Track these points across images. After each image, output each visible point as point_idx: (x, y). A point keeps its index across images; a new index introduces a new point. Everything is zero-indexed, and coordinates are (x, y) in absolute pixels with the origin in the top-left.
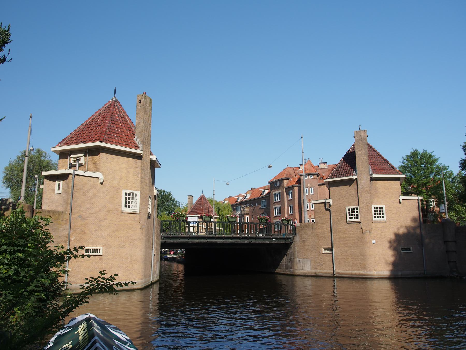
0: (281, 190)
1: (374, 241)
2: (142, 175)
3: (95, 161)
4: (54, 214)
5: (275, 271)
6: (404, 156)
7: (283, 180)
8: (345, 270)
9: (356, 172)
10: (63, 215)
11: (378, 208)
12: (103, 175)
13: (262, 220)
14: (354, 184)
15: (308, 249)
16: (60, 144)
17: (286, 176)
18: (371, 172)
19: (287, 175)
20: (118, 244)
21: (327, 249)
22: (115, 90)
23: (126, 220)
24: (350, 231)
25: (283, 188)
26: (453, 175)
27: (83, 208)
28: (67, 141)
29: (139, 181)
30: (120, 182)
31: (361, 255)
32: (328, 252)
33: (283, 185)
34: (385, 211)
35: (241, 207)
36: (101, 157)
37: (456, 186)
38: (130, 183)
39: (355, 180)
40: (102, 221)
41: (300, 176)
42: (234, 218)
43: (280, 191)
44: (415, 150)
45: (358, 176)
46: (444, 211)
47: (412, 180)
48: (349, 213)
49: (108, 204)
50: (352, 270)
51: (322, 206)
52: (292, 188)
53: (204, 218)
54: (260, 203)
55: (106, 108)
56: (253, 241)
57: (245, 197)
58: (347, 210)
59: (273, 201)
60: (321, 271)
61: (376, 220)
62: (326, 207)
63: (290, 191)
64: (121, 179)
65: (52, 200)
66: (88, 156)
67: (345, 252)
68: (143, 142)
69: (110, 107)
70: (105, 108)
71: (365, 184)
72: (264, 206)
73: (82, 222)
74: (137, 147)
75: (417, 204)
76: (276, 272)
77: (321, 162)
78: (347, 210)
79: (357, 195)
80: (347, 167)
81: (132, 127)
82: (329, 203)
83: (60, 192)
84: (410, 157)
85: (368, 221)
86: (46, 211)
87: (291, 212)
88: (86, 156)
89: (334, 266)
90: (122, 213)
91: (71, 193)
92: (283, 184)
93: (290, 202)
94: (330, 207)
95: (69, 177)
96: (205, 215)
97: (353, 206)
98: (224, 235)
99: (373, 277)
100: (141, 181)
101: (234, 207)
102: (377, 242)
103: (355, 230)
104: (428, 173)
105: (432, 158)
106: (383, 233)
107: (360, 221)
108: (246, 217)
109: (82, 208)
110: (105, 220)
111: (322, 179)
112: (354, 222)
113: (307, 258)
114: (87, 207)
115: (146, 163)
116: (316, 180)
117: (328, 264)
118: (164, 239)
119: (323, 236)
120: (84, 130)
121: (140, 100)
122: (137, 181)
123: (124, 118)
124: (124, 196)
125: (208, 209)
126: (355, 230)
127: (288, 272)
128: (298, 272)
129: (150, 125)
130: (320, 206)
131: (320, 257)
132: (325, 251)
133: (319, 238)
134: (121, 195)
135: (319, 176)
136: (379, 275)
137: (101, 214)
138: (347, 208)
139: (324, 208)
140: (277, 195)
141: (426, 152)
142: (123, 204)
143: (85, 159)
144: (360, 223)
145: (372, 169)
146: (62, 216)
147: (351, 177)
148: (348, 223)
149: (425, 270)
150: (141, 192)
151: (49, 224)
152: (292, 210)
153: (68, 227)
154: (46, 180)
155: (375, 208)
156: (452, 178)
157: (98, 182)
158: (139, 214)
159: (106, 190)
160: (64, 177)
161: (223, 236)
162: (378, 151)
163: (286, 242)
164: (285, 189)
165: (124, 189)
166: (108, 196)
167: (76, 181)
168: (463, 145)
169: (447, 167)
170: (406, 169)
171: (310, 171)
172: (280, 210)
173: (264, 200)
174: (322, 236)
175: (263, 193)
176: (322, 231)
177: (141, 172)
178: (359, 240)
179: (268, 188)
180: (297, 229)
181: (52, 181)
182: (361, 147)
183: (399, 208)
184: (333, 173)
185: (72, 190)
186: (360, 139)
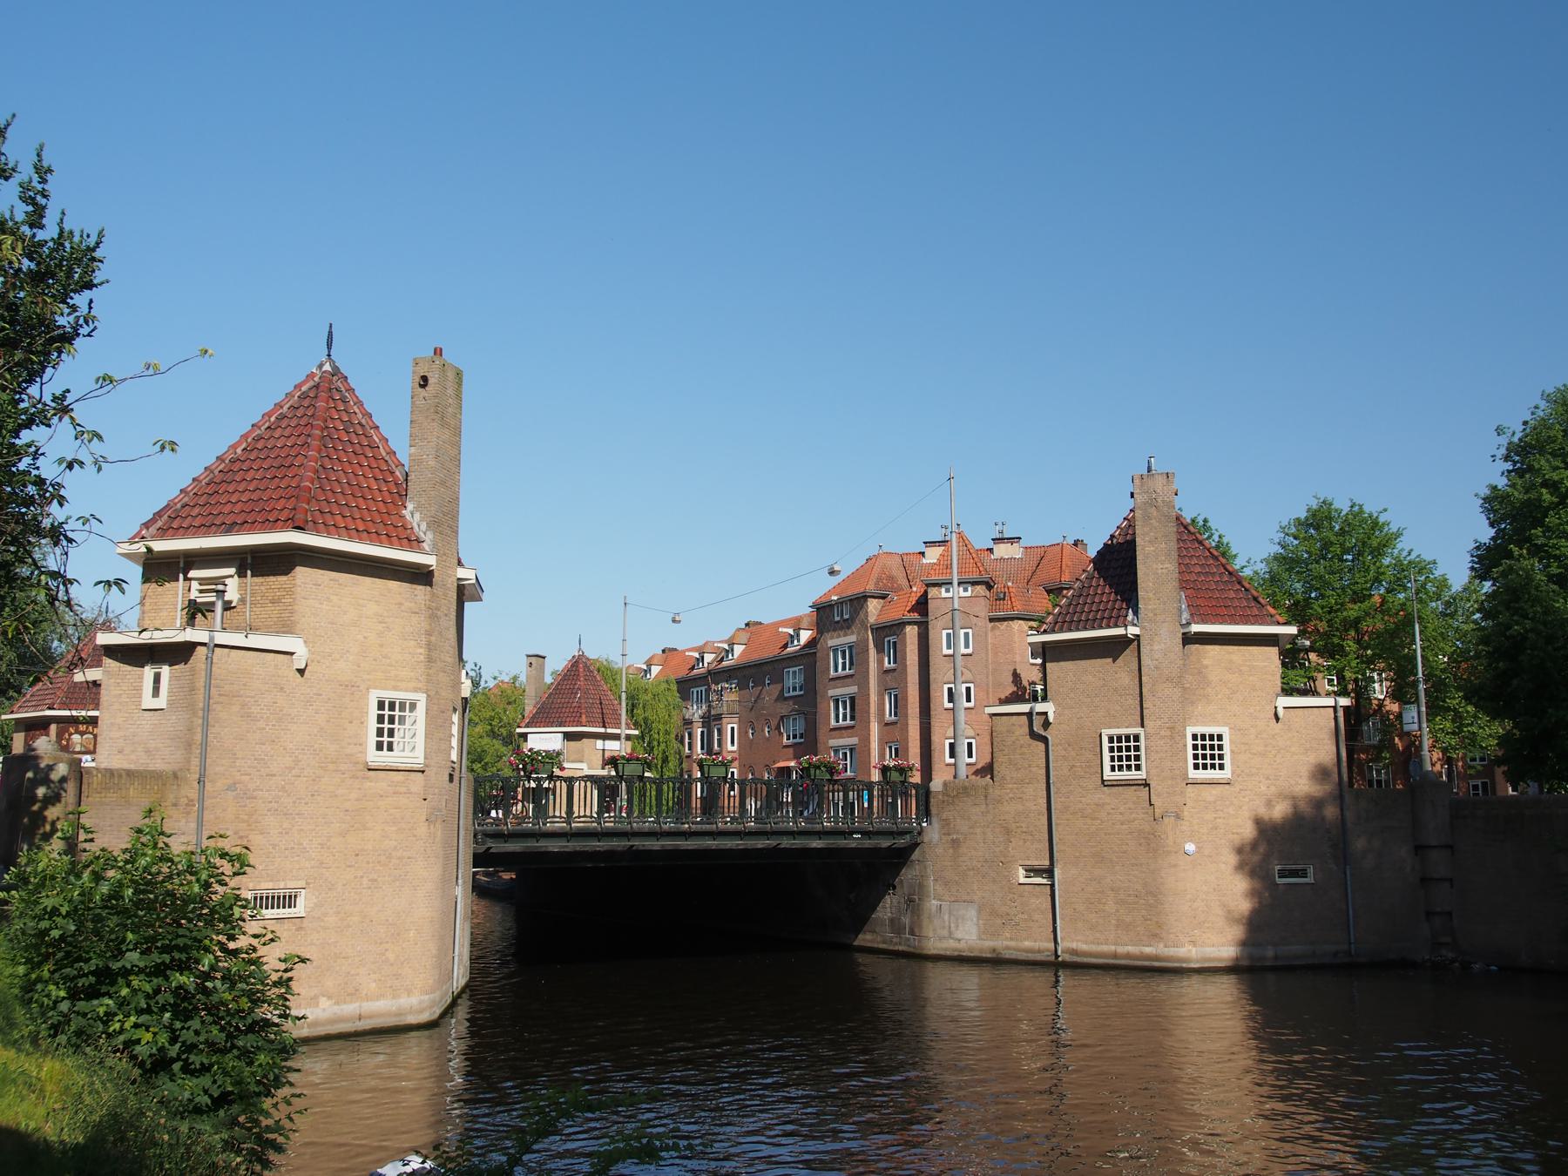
0: (859, 634)
1: (1190, 847)
2: (433, 639)
3: (278, 594)
4: (148, 782)
5: (854, 940)
9: (1136, 613)
10: (178, 785)
11: (1205, 735)
12: (305, 642)
13: (818, 771)
14: (1129, 654)
15: (969, 870)
16: (148, 528)
17: (877, 584)
18: (1186, 616)
19: (879, 579)
20: (356, 877)
21: (1032, 871)
22: (330, 333)
23: (381, 793)
24: (1112, 811)
25: (867, 626)
26: (1449, 588)
27: (243, 758)
28: (169, 517)
30: (362, 665)
33: (867, 619)
34: (1228, 738)
35: (708, 691)
36: (298, 582)
37: (1457, 630)
38: (392, 666)
40: (303, 801)
44: (1324, 502)
47: (1312, 609)
49: (324, 743)
51: (1021, 726)
52: (897, 627)
54: (778, 678)
55: (299, 397)
59: (829, 674)
60: (1012, 944)
61: (1197, 776)
62: (1035, 729)
64: (365, 652)
65: (131, 730)
66: (252, 576)
68: (435, 524)
69: (316, 397)
70: (296, 398)
72: (794, 689)
73: (240, 806)
74: (413, 543)
75: (1333, 724)
77: (1000, 536)
81: (394, 466)
82: (1046, 713)
83: (161, 702)
85: (1173, 778)
86: (124, 774)
88: (246, 576)
89: (1058, 928)
90: (369, 770)
91: (204, 710)
93: (889, 677)
94: (1045, 730)
95: (195, 653)
97: (1125, 730)
98: (688, 823)
99: (1184, 965)
100: (430, 660)
101: (686, 686)
103: (1130, 809)
107: (1145, 780)
108: (729, 726)
109: (238, 759)
110: (313, 795)
111: (1004, 599)
113: (968, 898)
114: (254, 755)
116: (983, 601)
117: (1037, 921)
119: (1022, 827)
120: (229, 477)
121: (425, 379)
122: (415, 659)
123: (366, 437)
124: (374, 712)
125: (601, 703)
126: (1130, 809)
127: (900, 944)
128: (934, 945)
129: (457, 461)
130: (1013, 725)
131: (1011, 896)
133: (1008, 832)
134: (365, 711)
135: (993, 587)
137: (300, 776)
138: (1106, 733)
139: (1027, 730)
140: (844, 652)
141: (1361, 511)
142: (373, 739)
143: (242, 588)
145: (1189, 606)
146: (175, 787)
147: (1119, 631)
148: (1105, 786)
150: (428, 696)
151: (244, 873)
152: (896, 707)
153: (193, 825)
154: (111, 661)
155: (1197, 735)
156: (1447, 598)
157: (287, 669)
158: (423, 772)
159: (314, 694)
160: (178, 653)
161: (687, 826)
163: (895, 843)
164: (872, 629)
165: (375, 688)
166: (323, 713)
167: (219, 668)
168: (1483, 496)
169: (1429, 563)
170: (1293, 569)
171: (964, 570)
173: (796, 669)
174: (1018, 825)
175: (792, 642)
176: (1020, 807)
177: (428, 627)
178: (1142, 841)
180: (932, 800)
181: (130, 665)
185: (205, 698)
186: (1152, 503)
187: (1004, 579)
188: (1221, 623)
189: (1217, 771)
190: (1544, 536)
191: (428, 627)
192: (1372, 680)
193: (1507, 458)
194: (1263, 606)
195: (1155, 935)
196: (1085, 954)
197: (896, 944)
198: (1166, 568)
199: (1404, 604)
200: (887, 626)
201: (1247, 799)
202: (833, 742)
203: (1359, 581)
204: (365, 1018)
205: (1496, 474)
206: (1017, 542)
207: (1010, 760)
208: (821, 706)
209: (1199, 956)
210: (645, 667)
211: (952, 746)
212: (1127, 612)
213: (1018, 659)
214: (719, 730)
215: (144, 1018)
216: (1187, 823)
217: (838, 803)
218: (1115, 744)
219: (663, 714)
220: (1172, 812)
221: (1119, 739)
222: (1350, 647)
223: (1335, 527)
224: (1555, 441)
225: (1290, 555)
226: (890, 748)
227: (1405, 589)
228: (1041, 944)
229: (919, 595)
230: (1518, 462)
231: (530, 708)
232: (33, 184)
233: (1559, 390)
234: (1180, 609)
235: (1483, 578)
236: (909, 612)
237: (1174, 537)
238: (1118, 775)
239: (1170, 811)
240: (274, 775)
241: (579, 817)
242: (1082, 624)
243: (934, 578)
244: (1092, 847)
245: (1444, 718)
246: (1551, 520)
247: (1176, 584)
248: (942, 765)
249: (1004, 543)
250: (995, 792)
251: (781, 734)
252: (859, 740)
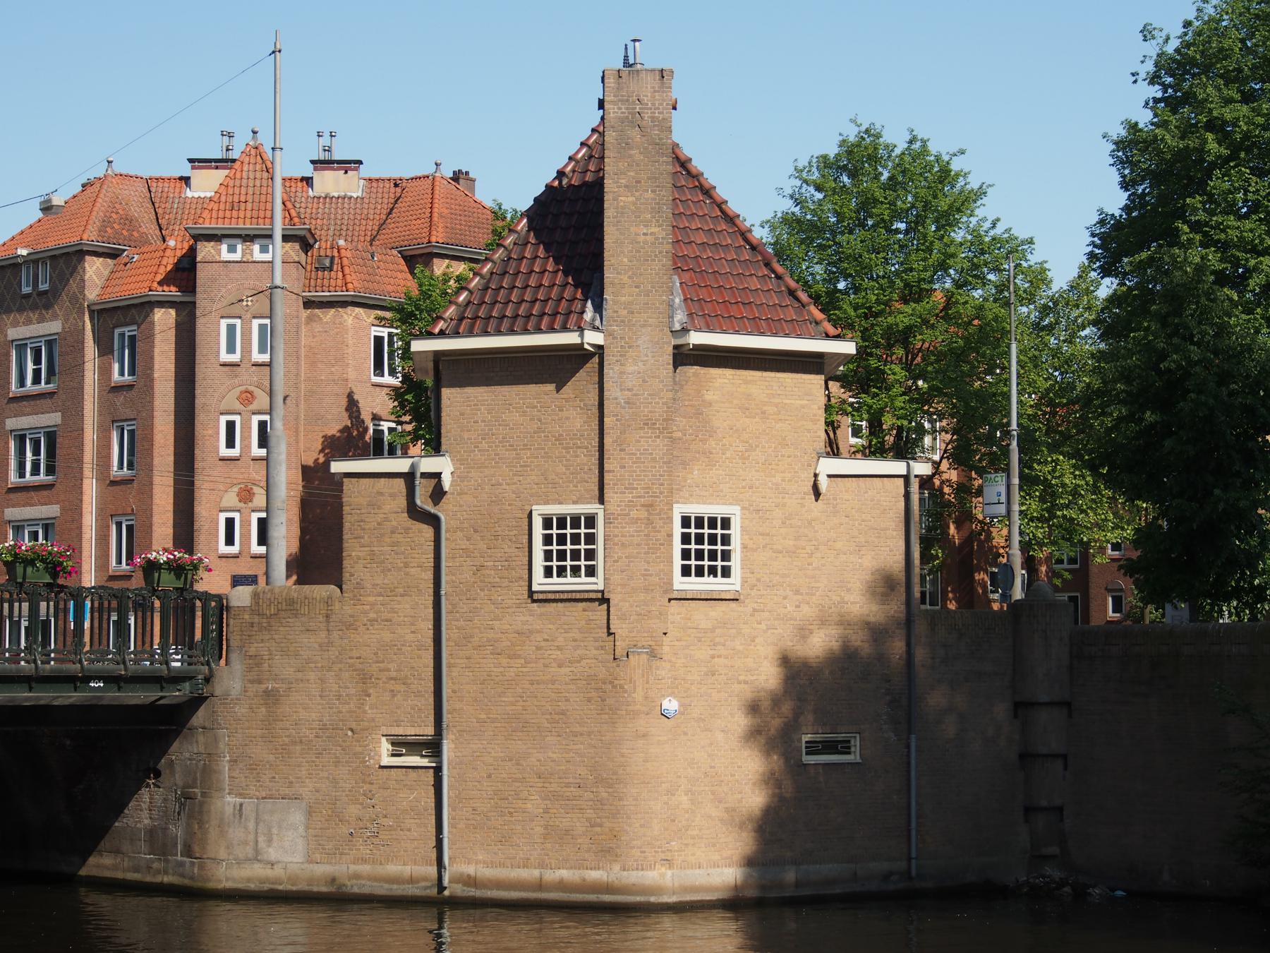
0: (66, 320)
1: (671, 705)
5: (80, 868)
6: (803, 163)
8: (502, 865)
9: (598, 308)
11: (716, 519)
13: (29, 570)
14: (584, 379)
15: (294, 743)
17: (102, 230)
18: (680, 318)
19: (106, 223)
21: (402, 745)
24: (543, 644)
26: (1048, 283)
32: (415, 760)
39: (592, 355)
41: (192, 242)
43: (53, 327)
44: (867, 131)
45: (609, 335)
46: (1002, 509)
47: (840, 308)
50: (542, 865)
51: (393, 496)
52: (140, 309)
58: (538, 523)
60: (365, 869)
62: (418, 502)
63: (126, 329)
67: (511, 760)
71: (644, 381)
78: (538, 523)
79: (595, 443)
82: (437, 476)
84: (839, 167)
87: (121, 466)
92: (83, 281)
93: (120, 399)
94: (436, 503)
99: (652, 899)
103: (575, 640)
105: (953, 187)
106: (719, 656)
107: (603, 592)
112: (570, 596)
117: (409, 830)
119: (389, 670)
126: (575, 640)
127: (166, 872)
130: (381, 494)
131: (366, 787)
132: (393, 755)
133: (365, 678)
135: (312, 246)
136: (686, 889)
138: (539, 511)
139: (402, 502)
141: (924, 151)
144: (604, 600)
145: (685, 300)
147: (570, 338)
148: (534, 601)
149: (914, 855)
162: (722, 192)
163: (162, 698)
164: (92, 312)
168: (1115, 138)
169: (1023, 243)
170: (812, 241)
172: (51, 454)
176: (387, 636)
178: (594, 694)
182: (638, 165)
183: (810, 523)
184: (469, 303)
187: (331, 233)
189: (719, 579)
192: (921, 431)
193: (1154, 79)
194: (803, 306)
195: (609, 850)
196: (499, 885)
197: (158, 872)
198: (651, 234)
199: (981, 308)
200: (118, 307)
201: (763, 626)
203: (915, 266)
206: (356, 169)
207: (372, 553)
209: (676, 884)
212: (584, 306)
213: (352, 374)
216: (668, 665)
217: (19, 622)
218: (555, 531)
220: (643, 647)
221: (562, 523)
222: (894, 374)
223: (881, 174)
225: (809, 217)
228: (416, 868)
229: (179, 254)
230: (1170, 86)
234: (671, 305)
235: (1106, 272)
236: (160, 283)
237: (667, 181)
239: (640, 644)
245: (1028, 494)
246: (1218, 184)
248: (213, 557)
249: (333, 169)
250: (345, 609)
252: (62, 509)
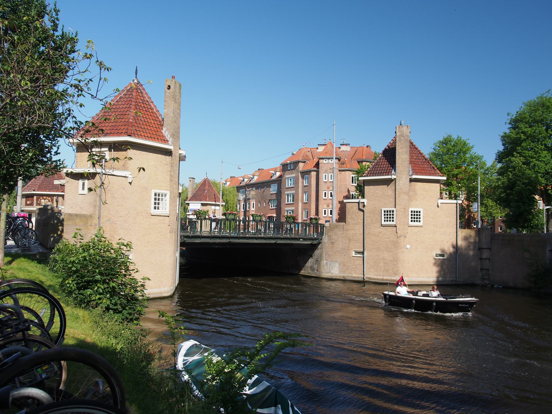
0: (296, 174)
1: (408, 246)
2: (172, 173)
7: (299, 162)
9: (395, 171)
14: (392, 184)
15: (337, 251)
17: (302, 158)
18: (411, 172)
19: (303, 156)
22: (137, 70)
29: (168, 180)
31: (394, 260)
39: (393, 180)
42: (260, 216)
45: (397, 176)
48: (385, 215)
50: (383, 276)
53: (227, 216)
56: (279, 242)
57: (251, 179)
58: (383, 212)
60: (350, 275)
62: (360, 208)
66: (114, 151)
68: (173, 136)
74: (166, 141)
76: (300, 273)
77: (343, 143)
78: (383, 212)
80: (386, 164)
82: (364, 203)
85: (404, 225)
86: (74, 215)
88: (111, 151)
96: (228, 213)
102: (411, 247)
104: (461, 162)
108: (252, 202)
111: (344, 164)
113: (335, 260)
115: (176, 159)
118: (183, 239)
121: (169, 86)
124: (153, 197)
128: (325, 275)
133: (350, 240)
139: (358, 208)
140: (291, 179)
141: (461, 139)
149: (457, 277)
150: (170, 192)
158: (169, 216)
161: (248, 235)
162: (419, 149)
164: (300, 173)
165: (154, 189)
168: (501, 136)
175: (274, 176)
176: (354, 232)
177: (170, 170)
178: (393, 244)
179: (280, 170)
188: (422, 175)
190: (521, 150)
191: (170, 170)
193: (510, 123)
202: (286, 209)
204: (151, 294)
205: (506, 129)
207: (351, 217)
208: (283, 196)
210: (225, 182)
211: (331, 211)
213: (347, 184)
214: (249, 204)
215: (101, 296)
219: (232, 198)
224: (526, 118)
226: (305, 211)
227: (473, 165)
230: (513, 125)
231: (190, 196)
232: (53, 15)
233: (529, 102)
234: (409, 170)
235: (499, 162)
238: (386, 223)
240: (122, 217)
241: (204, 231)
242: (377, 174)
243: (321, 157)
244: (377, 245)
247: (409, 162)
251: (269, 205)
